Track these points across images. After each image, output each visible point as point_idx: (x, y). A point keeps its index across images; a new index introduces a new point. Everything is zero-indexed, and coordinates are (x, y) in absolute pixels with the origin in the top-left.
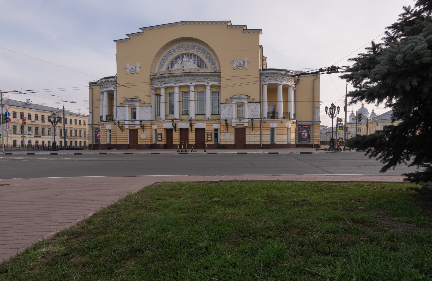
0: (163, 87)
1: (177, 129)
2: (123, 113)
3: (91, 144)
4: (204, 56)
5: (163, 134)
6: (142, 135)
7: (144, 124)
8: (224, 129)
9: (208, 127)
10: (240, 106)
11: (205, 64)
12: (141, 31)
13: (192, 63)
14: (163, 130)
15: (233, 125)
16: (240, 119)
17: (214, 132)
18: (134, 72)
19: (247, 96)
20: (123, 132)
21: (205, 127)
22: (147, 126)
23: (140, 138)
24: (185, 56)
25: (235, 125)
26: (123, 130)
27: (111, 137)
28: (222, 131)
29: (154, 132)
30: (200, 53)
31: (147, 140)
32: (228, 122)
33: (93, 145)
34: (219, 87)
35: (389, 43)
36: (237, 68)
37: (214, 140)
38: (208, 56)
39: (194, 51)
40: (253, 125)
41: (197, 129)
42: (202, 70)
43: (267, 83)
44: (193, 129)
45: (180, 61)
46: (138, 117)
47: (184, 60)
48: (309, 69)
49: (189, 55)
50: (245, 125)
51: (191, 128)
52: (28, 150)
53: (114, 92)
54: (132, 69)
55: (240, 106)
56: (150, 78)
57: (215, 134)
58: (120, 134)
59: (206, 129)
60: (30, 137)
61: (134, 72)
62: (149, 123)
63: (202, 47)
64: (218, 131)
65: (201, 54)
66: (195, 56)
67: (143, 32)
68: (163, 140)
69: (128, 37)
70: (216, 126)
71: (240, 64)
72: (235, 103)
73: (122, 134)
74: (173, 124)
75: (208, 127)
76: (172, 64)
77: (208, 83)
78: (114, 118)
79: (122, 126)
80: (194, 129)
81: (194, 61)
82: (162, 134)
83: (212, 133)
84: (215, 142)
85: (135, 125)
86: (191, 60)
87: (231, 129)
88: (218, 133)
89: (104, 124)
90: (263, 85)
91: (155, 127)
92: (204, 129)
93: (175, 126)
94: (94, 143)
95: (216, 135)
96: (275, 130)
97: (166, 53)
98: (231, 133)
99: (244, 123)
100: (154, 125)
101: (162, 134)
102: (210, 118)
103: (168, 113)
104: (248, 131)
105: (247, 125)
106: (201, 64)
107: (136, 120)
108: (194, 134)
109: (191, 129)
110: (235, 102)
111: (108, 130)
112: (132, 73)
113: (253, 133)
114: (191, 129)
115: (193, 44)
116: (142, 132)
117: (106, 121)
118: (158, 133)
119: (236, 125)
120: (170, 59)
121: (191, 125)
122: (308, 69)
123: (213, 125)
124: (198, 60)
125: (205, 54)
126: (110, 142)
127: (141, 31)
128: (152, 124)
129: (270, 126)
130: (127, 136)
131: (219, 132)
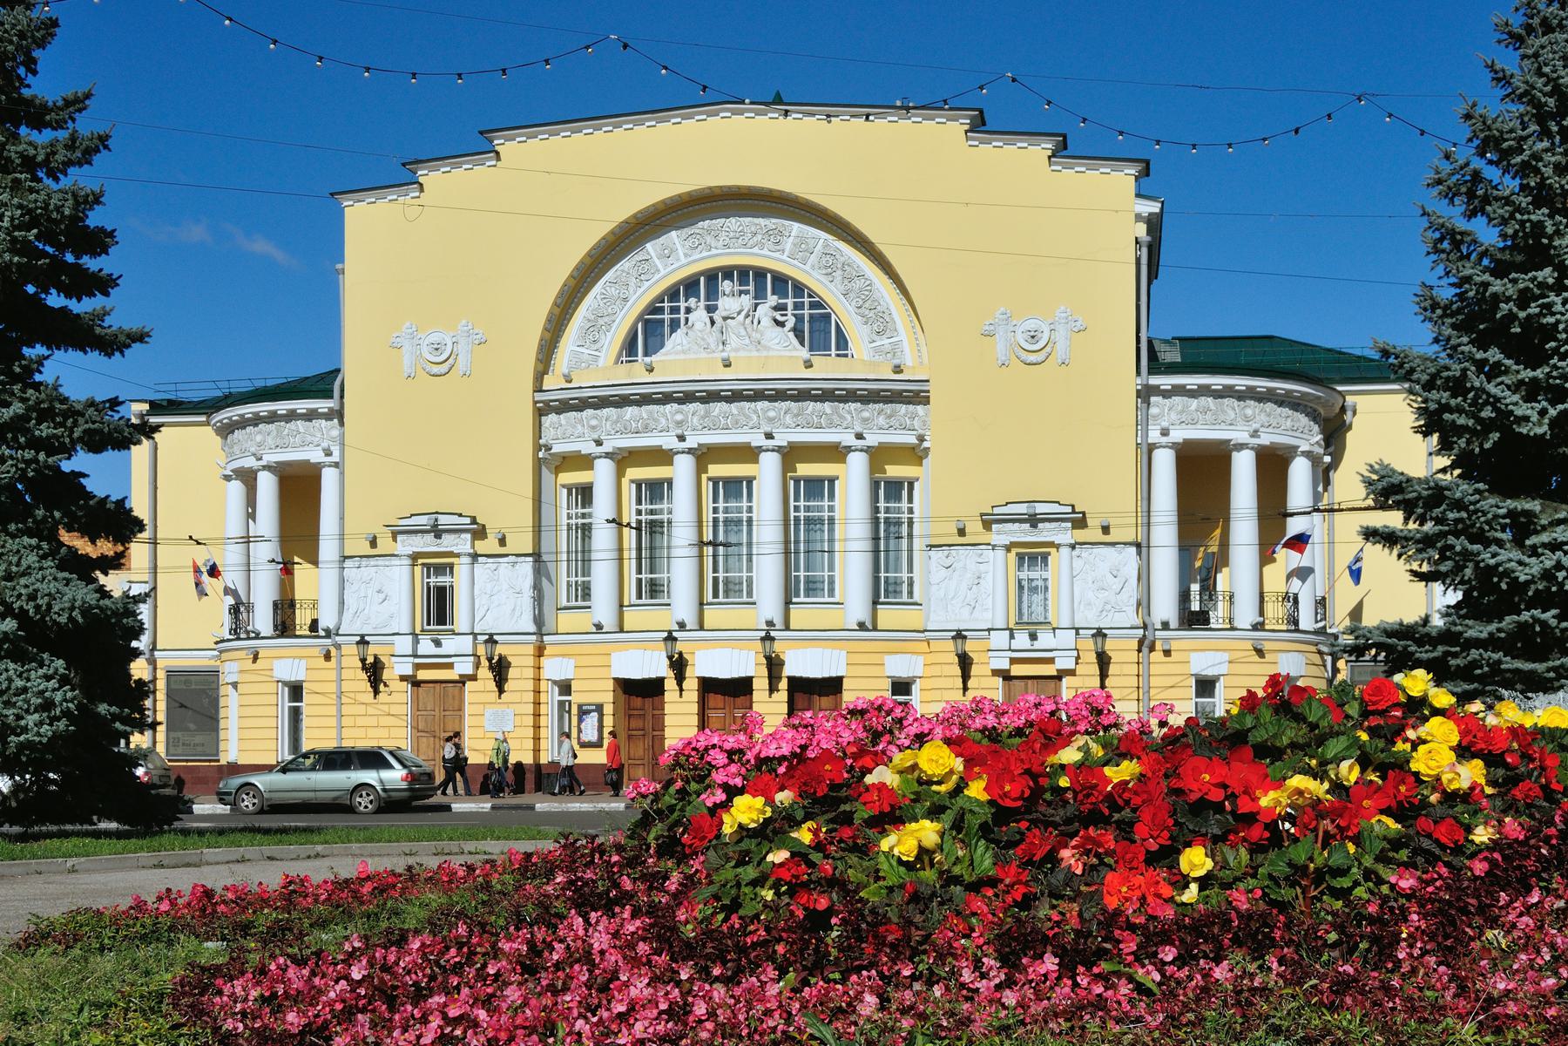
1: (691, 684)
4: (831, 286)
6: (489, 711)
9: (585, 673)
13: (766, 322)
14: (610, 685)
19: (1069, 509)
20: (381, 697)
21: (840, 674)
23: (479, 733)
29: (551, 697)
30: (813, 267)
32: (969, 647)
35: (1459, 237)
38: (859, 283)
39: (777, 255)
42: (827, 368)
43: (1178, 435)
45: (699, 316)
47: (726, 304)
51: (680, 678)
53: (317, 479)
56: (535, 403)
58: (361, 709)
59: (846, 684)
61: (444, 368)
65: (815, 274)
75: (585, 673)
77: (682, 438)
81: (780, 308)
82: (599, 708)
86: (765, 311)
90: (1151, 448)
93: (679, 665)
96: (915, 688)
101: (599, 708)
110: (1006, 540)
111: (285, 683)
118: (580, 706)
120: (640, 300)
122: (172, 387)
123: (888, 659)
124: (798, 306)
125: (839, 272)
129: (510, 711)
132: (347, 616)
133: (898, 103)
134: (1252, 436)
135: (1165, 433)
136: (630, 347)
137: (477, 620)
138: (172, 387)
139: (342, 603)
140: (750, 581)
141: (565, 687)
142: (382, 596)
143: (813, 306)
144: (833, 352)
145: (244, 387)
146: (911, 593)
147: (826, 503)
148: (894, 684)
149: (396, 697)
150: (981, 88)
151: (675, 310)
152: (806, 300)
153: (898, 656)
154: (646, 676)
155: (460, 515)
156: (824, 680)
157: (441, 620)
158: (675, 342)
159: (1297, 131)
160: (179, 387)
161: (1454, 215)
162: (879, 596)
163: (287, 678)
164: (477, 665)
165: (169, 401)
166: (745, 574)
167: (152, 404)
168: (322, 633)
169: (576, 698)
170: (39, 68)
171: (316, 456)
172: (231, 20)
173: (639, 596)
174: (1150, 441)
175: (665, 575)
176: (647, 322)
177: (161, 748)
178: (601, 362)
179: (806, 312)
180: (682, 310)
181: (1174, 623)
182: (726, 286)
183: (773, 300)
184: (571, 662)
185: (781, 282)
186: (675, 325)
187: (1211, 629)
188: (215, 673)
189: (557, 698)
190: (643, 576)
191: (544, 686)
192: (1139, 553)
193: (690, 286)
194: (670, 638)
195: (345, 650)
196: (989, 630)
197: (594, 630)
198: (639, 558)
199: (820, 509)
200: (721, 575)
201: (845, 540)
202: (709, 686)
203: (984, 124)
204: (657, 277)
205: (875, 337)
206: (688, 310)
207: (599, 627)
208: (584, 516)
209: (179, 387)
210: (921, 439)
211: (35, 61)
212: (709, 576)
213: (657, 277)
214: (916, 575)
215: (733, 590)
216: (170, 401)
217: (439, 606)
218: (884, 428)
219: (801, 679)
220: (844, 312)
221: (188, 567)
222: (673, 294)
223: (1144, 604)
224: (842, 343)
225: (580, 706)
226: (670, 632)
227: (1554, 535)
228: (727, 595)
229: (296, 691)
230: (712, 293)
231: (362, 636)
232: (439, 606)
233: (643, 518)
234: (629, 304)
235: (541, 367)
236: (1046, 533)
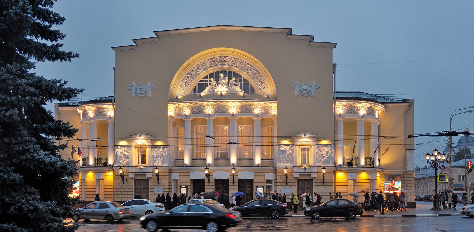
5: (189, 187)
6: (156, 187)
8: (282, 181)
9: (181, 177)
12: (133, 44)
14: (189, 181)
15: (295, 176)
19: (315, 135)
20: (126, 184)
24: (222, 75)
25: (298, 176)
26: (125, 180)
28: (278, 184)
36: (137, 95)
40: (158, 179)
44: (211, 181)
48: (82, 99)
50: (312, 176)
51: (209, 179)
59: (254, 181)
60: (102, 185)
64: (462, 180)
67: (136, 45)
71: (141, 90)
73: (123, 187)
80: (213, 181)
82: (445, 181)
85: (146, 174)
87: (292, 181)
98: (292, 187)
99: (311, 173)
100: (174, 173)
101: (445, 181)
102: (260, 166)
104: (316, 184)
105: (315, 176)
108: (238, 187)
109: (209, 181)
113: (324, 187)
114: (209, 181)
116: (157, 184)
117: (95, 167)
122: (81, 99)
127: (133, 44)
128: (170, 172)
141: (176, 181)
144: (250, 93)
145: (86, 100)
149: (130, 184)
152: (243, 79)
169: (179, 184)
170: (62, 16)
177: (305, 194)
179: (243, 82)
180: (209, 81)
185: (235, 75)
187: (353, 167)
193: (211, 75)
211: (56, 15)
221: (71, 147)
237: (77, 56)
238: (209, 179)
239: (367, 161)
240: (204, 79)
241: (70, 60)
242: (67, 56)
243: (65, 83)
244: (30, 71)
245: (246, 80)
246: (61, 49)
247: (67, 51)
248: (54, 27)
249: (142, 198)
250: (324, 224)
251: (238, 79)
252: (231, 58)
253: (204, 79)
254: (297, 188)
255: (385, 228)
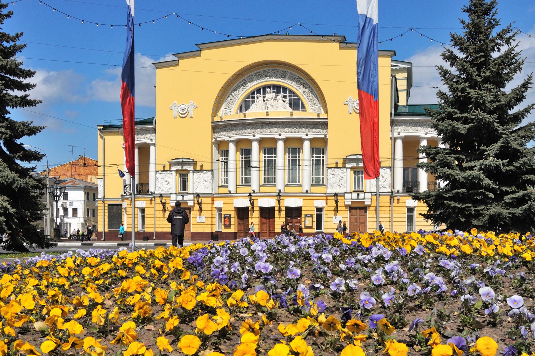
0: (282, 139)
2: (166, 181)
3: (102, 232)
4: (300, 90)
7: (201, 200)
10: (183, 175)
11: (302, 103)
13: (281, 101)
14: (233, 209)
16: (358, 193)
17: (315, 213)
18: (185, 116)
19: (192, 160)
22: (206, 203)
23: (195, 223)
24: (268, 90)
25: (350, 203)
27: (146, 219)
31: (206, 226)
33: (105, 232)
34: (324, 140)
37: (315, 227)
41: (287, 209)
42: (298, 114)
43: (403, 135)
44: (255, 209)
45: (261, 98)
46: (190, 190)
49: (277, 88)
52: (82, 240)
54: (183, 110)
55: (183, 175)
57: (317, 215)
59: (303, 209)
62: (210, 199)
63: (298, 75)
66: (285, 89)
68: (232, 226)
69: (176, 59)
70: (321, 203)
72: (175, 171)
74: (250, 201)
76: (246, 104)
77: (307, 135)
78: (151, 189)
79: (165, 202)
80: (258, 209)
83: (230, 215)
84: (317, 229)
86: (279, 97)
88: (321, 215)
89: (400, 201)
90: (395, 139)
91: (218, 204)
92: (299, 209)
93: (252, 203)
94: (107, 230)
95: (319, 219)
97: (238, 83)
99: (365, 200)
103: (240, 183)
105: (369, 203)
106: (296, 104)
107: (187, 193)
112: (182, 116)
115: (283, 69)
118: (224, 215)
119: (352, 202)
121: (252, 203)
122: (110, 121)
123: (315, 201)
126: (143, 227)
130: (418, 224)
131: (323, 213)
132: (157, 188)
133: (333, 35)
134: (426, 135)
135: (399, 133)
136: (240, 109)
137: (194, 190)
138: (110, 121)
139: (156, 184)
140: (299, 178)
141: (220, 210)
142: (167, 183)
143: (294, 96)
146: (323, 182)
147: (321, 156)
148: (408, 209)
150: (290, 28)
151: (253, 98)
153: (317, 201)
154: (244, 206)
155: (189, 159)
156: (296, 208)
157: (185, 190)
158: (253, 106)
159: (391, 40)
160: (112, 121)
161: (447, 65)
162: (313, 182)
163: (140, 207)
164: (195, 203)
165: (109, 125)
166: (314, 176)
167: (104, 126)
168: (150, 193)
169: (223, 213)
171: (148, 141)
172: (55, 9)
173: (265, 182)
174: (394, 136)
175: (250, 176)
176: (245, 101)
178: (232, 113)
179: (292, 98)
181: (401, 191)
182: (268, 90)
183: (282, 94)
184: (222, 202)
186: (254, 102)
188: (121, 205)
189: (140, 214)
190: (244, 177)
191: (136, 209)
192: (391, 171)
194: (250, 195)
195: (156, 198)
196: (345, 193)
197: (229, 193)
198: (265, 170)
199: (272, 157)
200: (321, 176)
201: (303, 165)
202: (262, 209)
203: (346, 41)
204: (248, 88)
205: (312, 105)
206: (258, 98)
207: (230, 192)
208: (246, 158)
209: (112, 121)
210: (325, 135)
212: (287, 176)
213: (248, 88)
214: (325, 176)
215: (270, 181)
216: (109, 125)
217: (184, 185)
218: (313, 133)
219: (289, 207)
220: (287, 70)
222: (253, 93)
223: (393, 185)
224: (303, 107)
225: (224, 215)
226: (250, 193)
227: (472, 164)
228: (268, 182)
229: (143, 210)
230: (265, 92)
231: (161, 194)
232: (184, 185)
233: (290, 158)
234: (240, 96)
235: (214, 115)
236: (186, 167)
237: (41, 102)
238: (253, 208)
239: (431, 185)
240: (251, 96)
241: (35, 106)
242: (31, 103)
243: (32, 122)
244: (7, 116)
245: (297, 96)
246: (28, 98)
247: (32, 100)
248: (25, 81)
249: (120, 211)
250: (164, 214)
251: (287, 95)
252: (279, 71)
253: (251, 96)
254: (350, 217)
255: (101, 200)
